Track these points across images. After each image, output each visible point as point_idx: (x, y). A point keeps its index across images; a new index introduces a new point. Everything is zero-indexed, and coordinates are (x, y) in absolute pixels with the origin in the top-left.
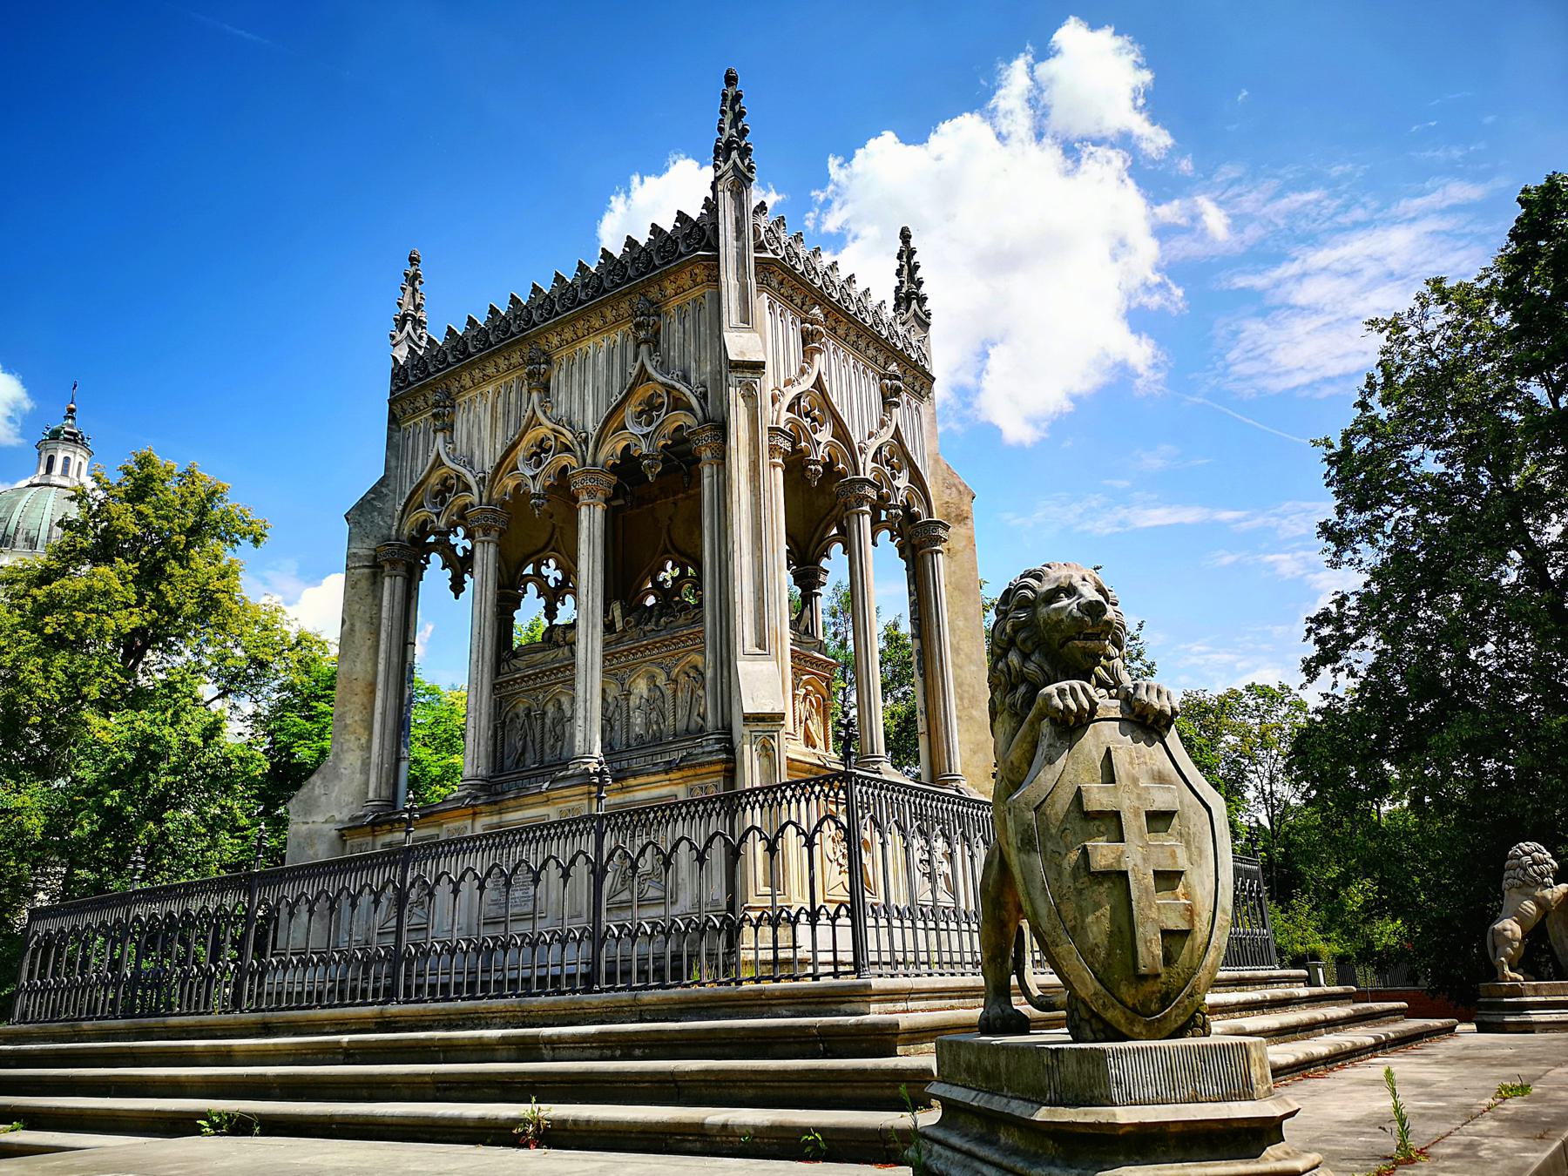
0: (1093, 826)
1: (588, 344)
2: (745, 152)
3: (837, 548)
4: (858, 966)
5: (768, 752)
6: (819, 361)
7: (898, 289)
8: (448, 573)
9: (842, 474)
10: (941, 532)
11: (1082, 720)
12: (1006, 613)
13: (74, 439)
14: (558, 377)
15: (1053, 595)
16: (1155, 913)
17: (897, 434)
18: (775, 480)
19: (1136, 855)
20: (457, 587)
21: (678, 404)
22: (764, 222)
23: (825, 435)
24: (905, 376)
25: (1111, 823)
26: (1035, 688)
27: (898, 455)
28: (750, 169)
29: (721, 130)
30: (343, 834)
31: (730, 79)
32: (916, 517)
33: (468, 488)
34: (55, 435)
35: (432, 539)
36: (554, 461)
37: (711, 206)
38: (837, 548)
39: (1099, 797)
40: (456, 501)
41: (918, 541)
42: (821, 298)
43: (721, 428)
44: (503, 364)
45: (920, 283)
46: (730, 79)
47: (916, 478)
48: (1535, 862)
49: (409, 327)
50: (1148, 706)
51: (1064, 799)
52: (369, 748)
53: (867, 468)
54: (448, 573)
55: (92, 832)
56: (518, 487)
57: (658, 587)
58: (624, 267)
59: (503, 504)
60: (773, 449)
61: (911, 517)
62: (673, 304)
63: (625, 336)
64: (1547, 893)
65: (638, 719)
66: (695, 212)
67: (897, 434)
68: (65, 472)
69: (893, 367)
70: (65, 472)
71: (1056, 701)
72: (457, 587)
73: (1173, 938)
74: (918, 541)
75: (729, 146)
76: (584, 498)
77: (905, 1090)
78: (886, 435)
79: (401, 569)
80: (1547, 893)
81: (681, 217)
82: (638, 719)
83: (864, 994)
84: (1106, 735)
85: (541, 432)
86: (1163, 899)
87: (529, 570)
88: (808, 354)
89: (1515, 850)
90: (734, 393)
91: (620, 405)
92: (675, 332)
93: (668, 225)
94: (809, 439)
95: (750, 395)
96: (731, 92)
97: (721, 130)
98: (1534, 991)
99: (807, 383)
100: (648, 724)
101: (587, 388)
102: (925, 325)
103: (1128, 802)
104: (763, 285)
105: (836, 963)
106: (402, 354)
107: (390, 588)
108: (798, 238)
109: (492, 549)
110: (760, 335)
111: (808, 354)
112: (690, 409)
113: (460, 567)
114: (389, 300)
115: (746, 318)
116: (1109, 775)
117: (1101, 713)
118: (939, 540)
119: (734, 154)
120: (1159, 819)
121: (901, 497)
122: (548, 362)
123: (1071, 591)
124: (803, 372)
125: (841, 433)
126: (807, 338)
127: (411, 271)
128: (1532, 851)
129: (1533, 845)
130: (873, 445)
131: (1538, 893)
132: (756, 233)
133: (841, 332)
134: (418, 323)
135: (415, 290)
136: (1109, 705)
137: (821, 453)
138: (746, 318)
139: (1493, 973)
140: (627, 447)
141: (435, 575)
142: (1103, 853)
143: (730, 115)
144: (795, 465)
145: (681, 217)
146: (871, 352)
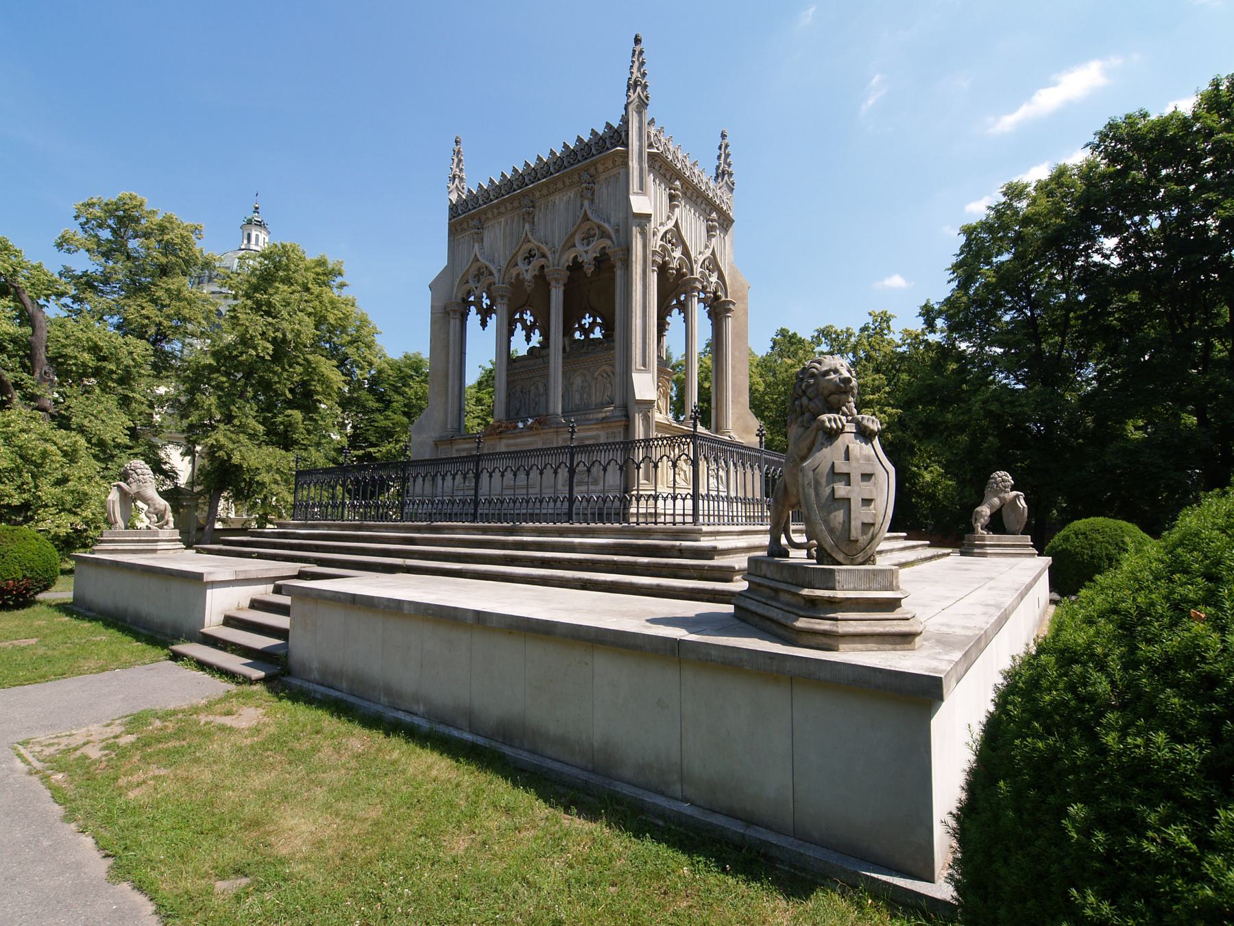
0: (837, 478)
1: (556, 198)
2: (645, 87)
3: (675, 311)
4: (695, 522)
5: (647, 419)
6: (677, 210)
7: (718, 167)
8: (479, 317)
9: (684, 275)
10: (731, 306)
11: (840, 431)
12: (802, 379)
13: (260, 224)
14: (539, 215)
15: (827, 373)
16: (860, 515)
17: (713, 253)
18: (653, 278)
19: (855, 491)
20: (484, 324)
21: (604, 234)
22: (653, 131)
23: (677, 254)
24: (719, 220)
25: (846, 478)
26: (815, 416)
27: (713, 264)
28: (647, 98)
29: (632, 73)
30: (437, 444)
31: (637, 41)
32: (719, 298)
33: (491, 274)
34: (250, 222)
35: (472, 299)
36: (536, 262)
37: (625, 121)
38: (675, 311)
39: (841, 467)
40: (485, 280)
41: (718, 310)
42: (678, 175)
43: (627, 250)
44: (509, 206)
45: (729, 165)
46: (637, 41)
47: (721, 277)
48: (1003, 481)
49: (457, 181)
50: (866, 427)
51: (825, 469)
52: (446, 403)
53: (697, 269)
54: (479, 317)
55: (1204, 761)
56: (518, 275)
57: (582, 327)
58: (576, 154)
59: (511, 284)
60: (654, 262)
61: (716, 298)
62: (603, 177)
63: (576, 195)
64: (1006, 496)
65: (577, 396)
66: (616, 124)
67: (713, 253)
68: (257, 244)
69: (714, 215)
70: (257, 244)
71: (827, 424)
72: (484, 324)
73: (867, 526)
74: (718, 310)
75: (636, 84)
76: (553, 283)
77: (726, 574)
78: (708, 253)
79: (458, 316)
80: (1006, 496)
81: (608, 126)
82: (577, 396)
83: (700, 532)
84: (848, 439)
85: (530, 246)
86: (864, 510)
87: (517, 316)
88: (672, 208)
89: (994, 475)
90: (635, 230)
91: (573, 235)
92: (603, 191)
93: (600, 131)
94: (670, 256)
95: (644, 234)
96: (638, 48)
97: (632, 73)
98: (991, 538)
99: (670, 224)
100: (582, 399)
101: (556, 220)
102: (731, 190)
103: (855, 471)
104: (652, 167)
105: (684, 515)
106: (454, 197)
107: (454, 323)
108: (695, 164)
109: (505, 307)
110: (647, 199)
111: (672, 208)
112: (610, 238)
113: (485, 314)
114: (447, 166)
115: (642, 187)
116: (847, 458)
117: (846, 429)
118: (729, 310)
119: (639, 89)
120: (867, 477)
121: (712, 288)
122: (533, 207)
123: (836, 371)
124: (669, 218)
125: (686, 252)
126: (672, 198)
127: (456, 148)
128: (1003, 477)
129: (1003, 473)
130: (701, 258)
131: (1002, 495)
132: (649, 136)
133: (689, 194)
134: (461, 179)
135: (460, 161)
136: (851, 428)
137: (675, 264)
138: (642, 187)
139: (972, 530)
140: (576, 257)
141: (473, 318)
142: (841, 490)
143: (637, 64)
144: (663, 269)
145: (608, 126)
146: (703, 206)
